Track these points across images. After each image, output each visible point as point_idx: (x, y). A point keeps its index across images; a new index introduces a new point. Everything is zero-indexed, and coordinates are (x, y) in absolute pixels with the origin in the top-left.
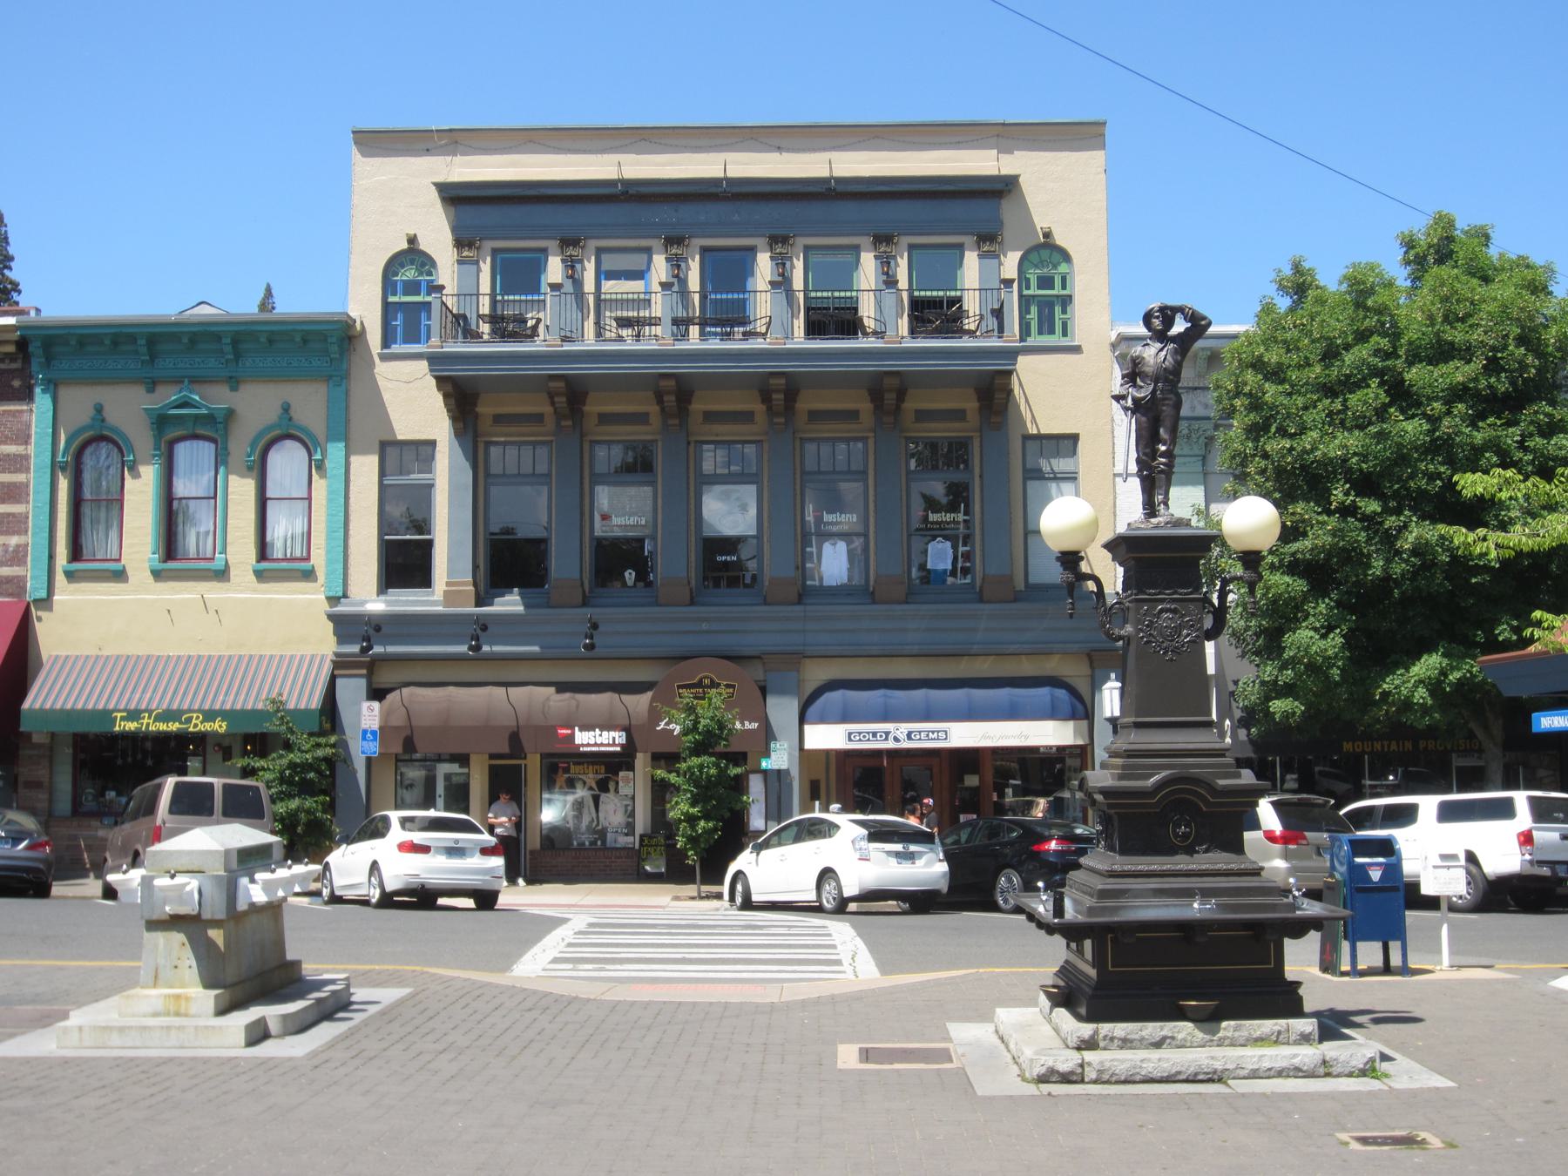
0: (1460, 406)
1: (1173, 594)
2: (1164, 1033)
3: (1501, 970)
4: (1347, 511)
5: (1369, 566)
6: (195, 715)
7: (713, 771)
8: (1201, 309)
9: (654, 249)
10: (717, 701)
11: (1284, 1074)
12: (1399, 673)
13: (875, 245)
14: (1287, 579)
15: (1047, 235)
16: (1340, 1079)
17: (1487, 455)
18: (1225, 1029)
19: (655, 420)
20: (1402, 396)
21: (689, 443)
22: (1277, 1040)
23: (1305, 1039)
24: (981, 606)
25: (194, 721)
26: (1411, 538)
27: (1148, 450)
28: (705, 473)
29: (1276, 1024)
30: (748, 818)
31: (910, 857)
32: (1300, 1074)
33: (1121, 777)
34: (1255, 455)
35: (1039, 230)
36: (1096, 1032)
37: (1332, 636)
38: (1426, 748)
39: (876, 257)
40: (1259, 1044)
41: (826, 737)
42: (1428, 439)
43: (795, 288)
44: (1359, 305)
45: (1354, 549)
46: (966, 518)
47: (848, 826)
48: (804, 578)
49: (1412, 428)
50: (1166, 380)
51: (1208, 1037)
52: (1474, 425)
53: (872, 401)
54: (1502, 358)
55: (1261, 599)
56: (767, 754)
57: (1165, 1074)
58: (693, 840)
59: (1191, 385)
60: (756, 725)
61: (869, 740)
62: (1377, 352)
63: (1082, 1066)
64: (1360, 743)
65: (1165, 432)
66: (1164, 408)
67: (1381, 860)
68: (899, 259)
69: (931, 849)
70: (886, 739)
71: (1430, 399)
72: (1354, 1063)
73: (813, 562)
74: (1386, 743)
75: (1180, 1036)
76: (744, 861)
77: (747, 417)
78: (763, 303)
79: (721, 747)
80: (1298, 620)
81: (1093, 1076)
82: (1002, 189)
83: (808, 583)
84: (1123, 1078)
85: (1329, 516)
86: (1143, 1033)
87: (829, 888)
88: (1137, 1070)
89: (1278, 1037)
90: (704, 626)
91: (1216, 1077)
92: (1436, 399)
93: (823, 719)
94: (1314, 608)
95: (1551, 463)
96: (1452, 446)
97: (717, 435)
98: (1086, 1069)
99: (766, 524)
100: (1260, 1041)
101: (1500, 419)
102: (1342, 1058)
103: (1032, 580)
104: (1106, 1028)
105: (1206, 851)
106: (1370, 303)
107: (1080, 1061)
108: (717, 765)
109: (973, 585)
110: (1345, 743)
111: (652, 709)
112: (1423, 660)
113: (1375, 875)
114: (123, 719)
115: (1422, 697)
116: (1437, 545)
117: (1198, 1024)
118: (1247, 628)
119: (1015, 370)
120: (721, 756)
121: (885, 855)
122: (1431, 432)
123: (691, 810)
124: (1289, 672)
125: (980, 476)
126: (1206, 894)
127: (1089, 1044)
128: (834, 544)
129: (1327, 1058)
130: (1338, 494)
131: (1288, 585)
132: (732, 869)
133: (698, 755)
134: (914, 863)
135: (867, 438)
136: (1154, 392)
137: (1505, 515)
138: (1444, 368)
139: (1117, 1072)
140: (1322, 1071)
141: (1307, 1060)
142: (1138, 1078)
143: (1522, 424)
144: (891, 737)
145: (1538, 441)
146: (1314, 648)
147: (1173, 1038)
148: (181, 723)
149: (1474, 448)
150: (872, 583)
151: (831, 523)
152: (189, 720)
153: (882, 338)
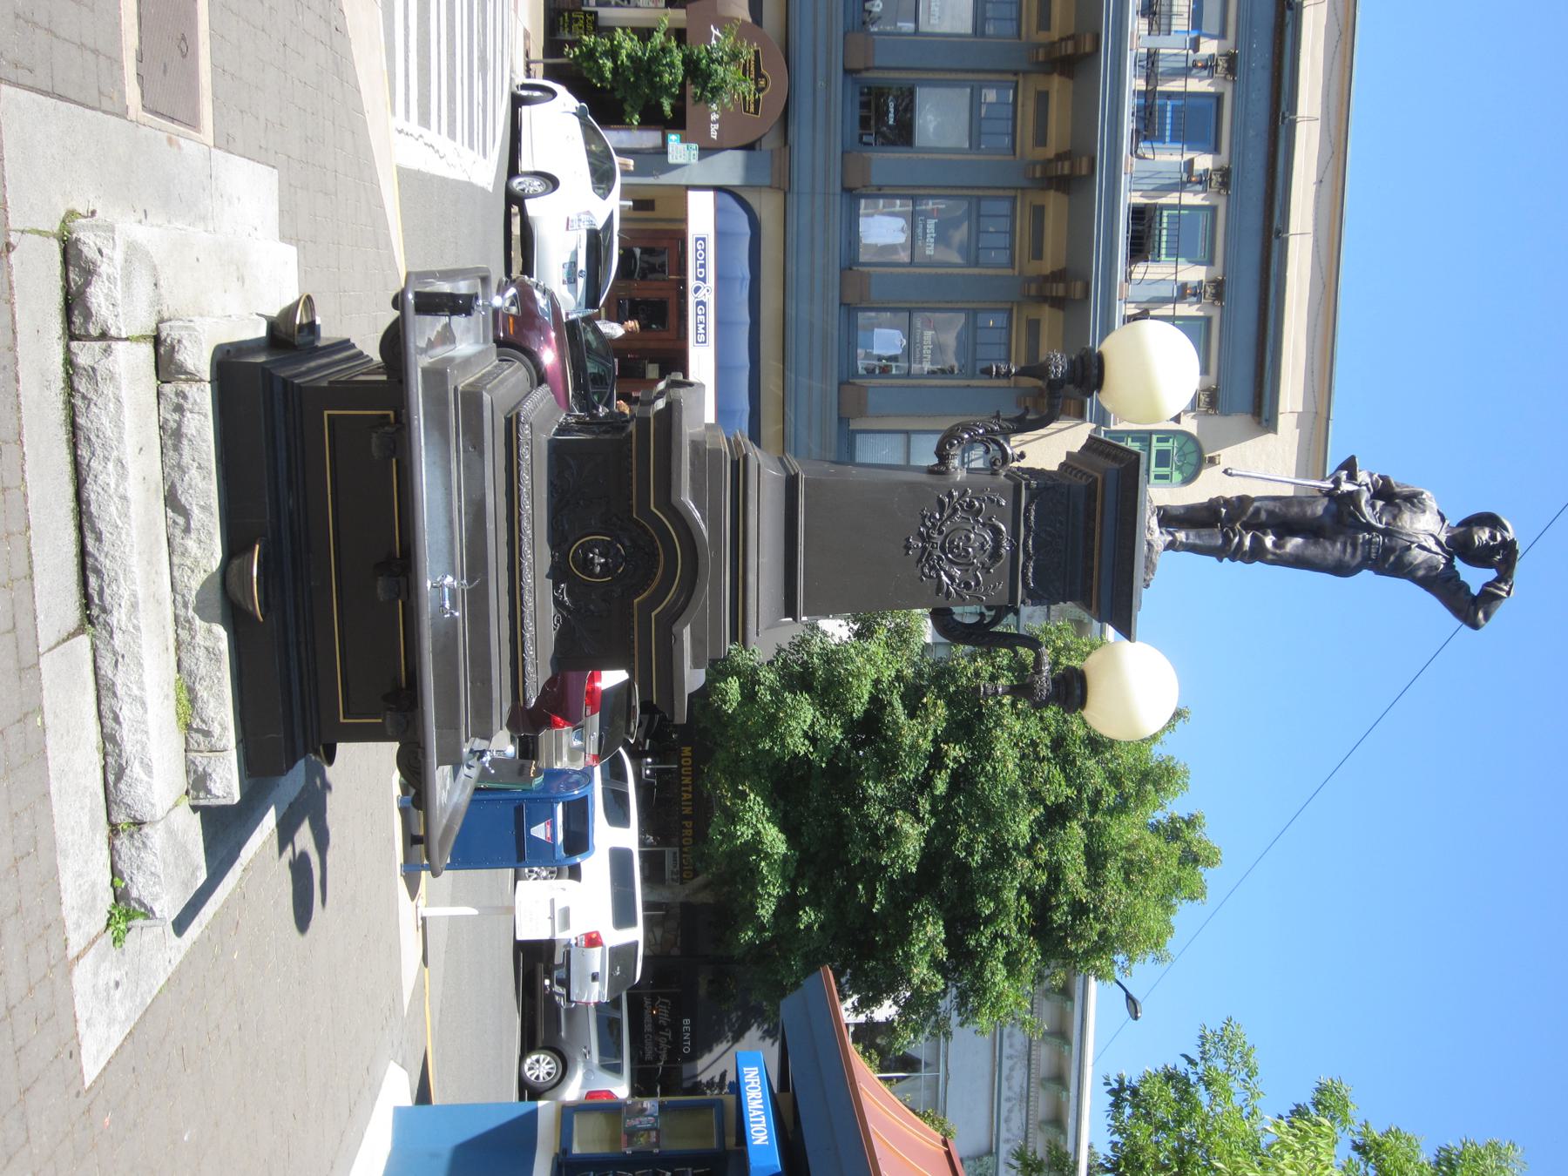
0: (1044, 878)
1: (1026, 552)
2: (196, 512)
3: (420, 985)
4: (936, 759)
5: (877, 781)
7: (667, 78)
8: (1501, 612)
9: (1223, 42)
10: (743, 88)
11: (109, 747)
12: (766, 810)
13: (1213, 282)
14: (866, 697)
15: (1212, 461)
16: (106, 852)
17: (992, 905)
18: (210, 631)
19: (1043, 37)
20: (1056, 816)
21: (1016, 73)
22: (192, 728)
23: (198, 781)
24: (835, 383)
26: (906, 826)
27: (1263, 516)
28: (984, 91)
29: (224, 728)
30: (614, 129)
31: (571, 280)
32: (111, 778)
33: (696, 446)
34: (994, 667)
35: (1217, 453)
36: (192, 378)
37: (806, 742)
38: (684, 827)
39: (1200, 283)
40: (184, 696)
41: (701, 215)
42: (1010, 845)
44: (1145, 776)
45: (896, 766)
47: (609, 208)
48: (867, 196)
49: (1022, 827)
50: (1388, 550)
51: (192, 598)
52: (1022, 890)
53: (1053, 273)
54: (1088, 918)
55: (846, 670)
56: (683, 140)
57: (94, 509)
58: (590, 54)
60: (715, 137)
61: (697, 259)
62: (1098, 793)
63: (104, 336)
64: (683, 760)
65: (1297, 546)
66: (1339, 545)
68: (1197, 306)
69: (580, 304)
70: (698, 279)
71: (1051, 846)
72: (140, 879)
73: (884, 207)
74: (690, 789)
75: (191, 544)
76: (566, 101)
77: (1041, 139)
78: (1168, 158)
79: (692, 90)
80: (822, 707)
81: (83, 359)
82: (1262, 414)
83: (863, 202)
84: (81, 421)
85: (932, 741)
86: (194, 472)
87: (536, 185)
88: (99, 452)
89: (198, 730)
90: (821, 84)
91: (95, 611)
92: (1051, 854)
93: (719, 210)
94: (836, 724)
95: (978, 963)
96: (1001, 867)
97: (1023, 106)
98: (98, 346)
99: (926, 156)
100: (189, 697)
101: (1028, 917)
102: (148, 858)
103: (859, 438)
104: (202, 397)
105: (558, 603)
106: (1149, 787)
107: (113, 332)
108: (671, 84)
109: (856, 375)
110: (690, 748)
111: (731, 20)
112: (780, 835)
113: (540, 831)
115: (742, 834)
116: (899, 852)
117: (218, 579)
118: (810, 655)
119: (1085, 421)
120: (683, 86)
121: (574, 248)
122: (1016, 846)
123: (624, 52)
124: (769, 697)
125: (968, 386)
126: (477, 600)
127: (166, 365)
128: (902, 230)
129: (146, 829)
130: (955, 752)
131: (859, 698)
132: (560, 89)
133: (683, 62)
134: (564, 282)
135: (1013, 268)
136: (1369, 528)
137: (928, 921)
138: (1081, 860)
139: (94, 409)
140: (121, 818)
141: (140, 790)
142: (84, 452)
143: (1019, 936)
144: (700, 283)
145: (1002, 952)
146: (794, 724)
147: (187, 530)
149: (999, 890)
150: (861, 269)
151: (925, 228)
153: (1126, 281)
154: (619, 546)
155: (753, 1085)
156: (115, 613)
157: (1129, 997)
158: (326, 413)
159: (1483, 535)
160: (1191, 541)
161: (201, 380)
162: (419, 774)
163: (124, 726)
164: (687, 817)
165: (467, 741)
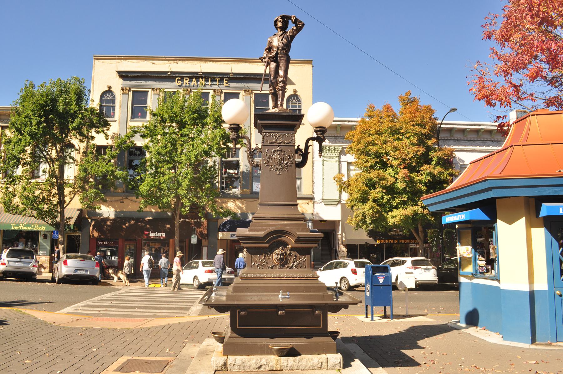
6: (36, 225)
25: (35, 227)
38: (401, 242)
43: (528, 347)
59: (335, 136)
67: (383, 274)
87: (196, 281)
114: (14, 226)
148: (32, 227)
152: (34, 227)
155: (450, 219)
157: (450, 112)
158: (237, 328)
159: (279, 24)
160: (280, 100)
162: (330, 305)
164: (398, 241)
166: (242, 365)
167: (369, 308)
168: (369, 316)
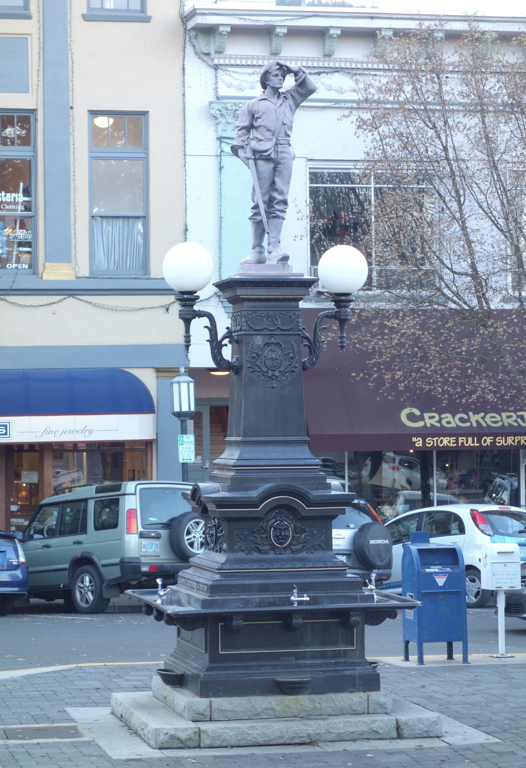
33: (230, 490)
46: (26, 199)
67: (448, 570)
154: (275, 524)
156: (309, 732)
161: (210, 701)
163: (355, 730)
165: (364, 593)
166: (271, 241)
167: (413, 646)
168: (413, 658)
